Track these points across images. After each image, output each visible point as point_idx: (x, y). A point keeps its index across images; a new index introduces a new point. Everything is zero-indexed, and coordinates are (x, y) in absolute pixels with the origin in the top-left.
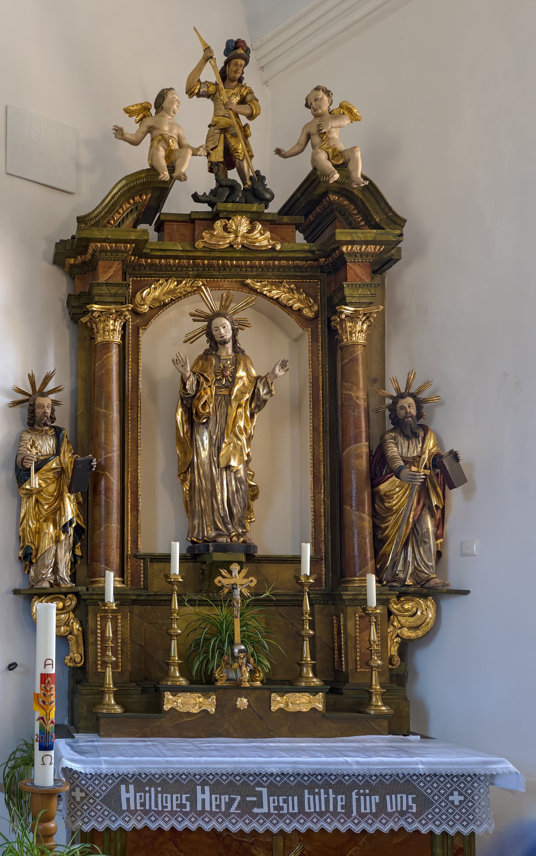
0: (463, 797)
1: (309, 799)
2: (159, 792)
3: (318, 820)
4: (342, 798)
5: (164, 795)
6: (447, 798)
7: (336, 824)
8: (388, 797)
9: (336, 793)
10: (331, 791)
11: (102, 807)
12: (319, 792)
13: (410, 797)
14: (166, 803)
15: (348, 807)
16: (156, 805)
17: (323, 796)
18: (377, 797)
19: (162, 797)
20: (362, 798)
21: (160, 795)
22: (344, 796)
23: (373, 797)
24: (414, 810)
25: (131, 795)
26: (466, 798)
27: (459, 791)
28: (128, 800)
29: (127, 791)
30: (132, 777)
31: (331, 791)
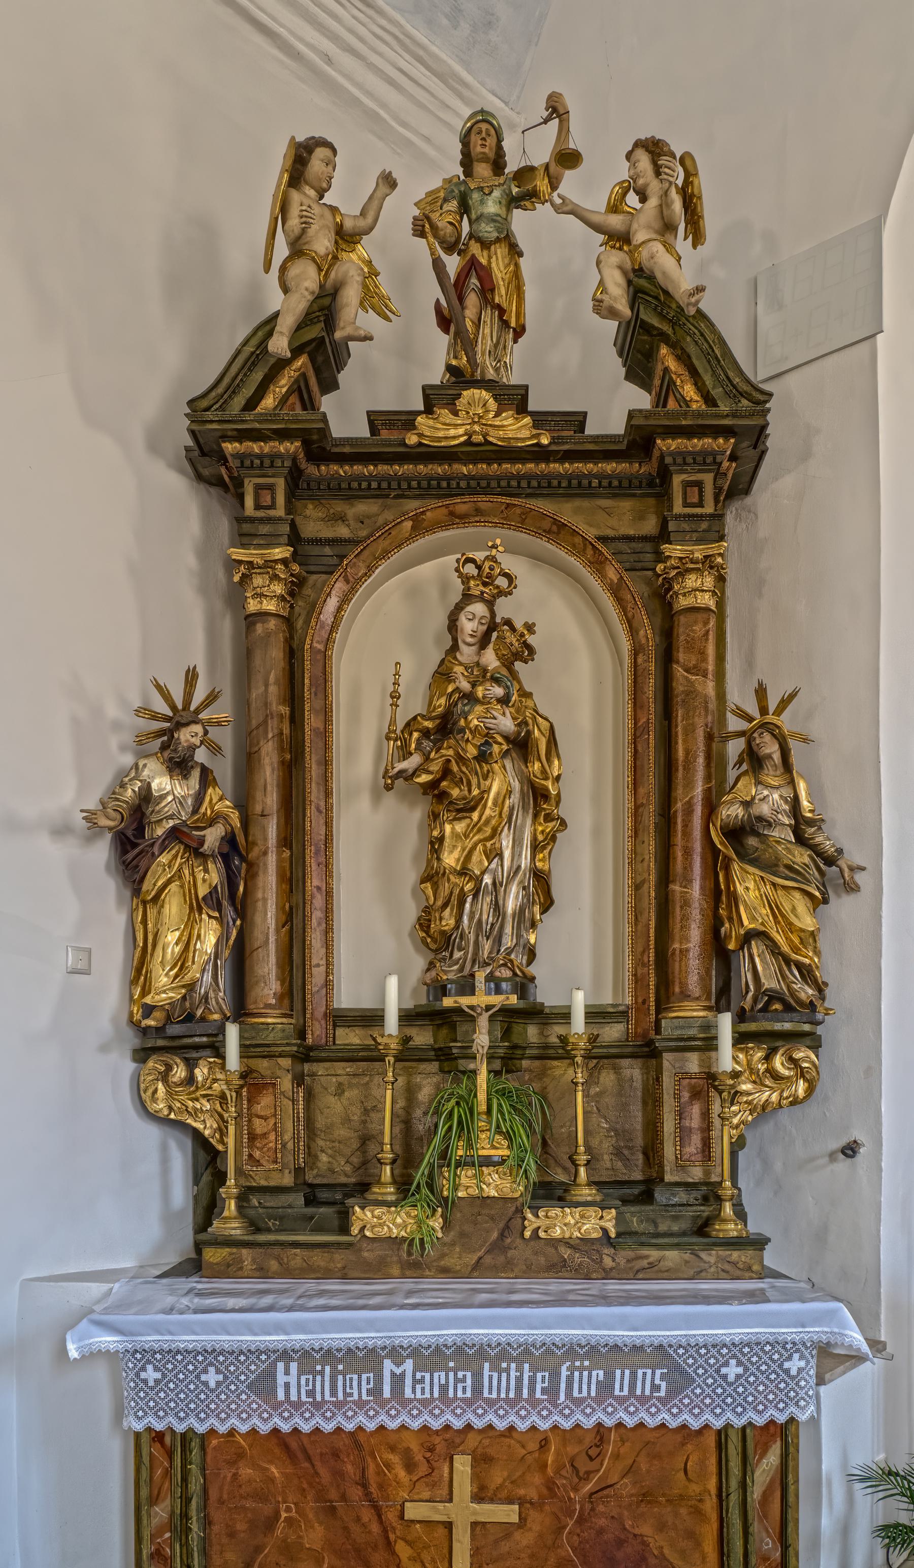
0: (142, 1377)
1: (491, 1377)
2: (340, 1372)
3: (637, 1409)
4: (543, 1377)
5: (348, 1377)
6: (198, 1377)
7: (556, 1417)
8: (618, 1372)
9: (534, 1369)
10: (526, 1366)
11: (249, 1397)
12: (323, 1370)
13: (658, 1372)
14: (351, 1388)
15: (552, 1391)
16: (334, 1392)
17: (513, 1374)
18: (601, 1373)
19: (345, 1380)
20: (577, 1374)
21: (340, 1377)
22: (372, 1375)
23: (436, 1375)
24: (662, 1393)
25: (293, 1380)
26: (226, 1377)
27: (216, 1367)
28: (287, 1385)
29: (287, 1373)
30: (541, 1347)
31: (526, 1366)
